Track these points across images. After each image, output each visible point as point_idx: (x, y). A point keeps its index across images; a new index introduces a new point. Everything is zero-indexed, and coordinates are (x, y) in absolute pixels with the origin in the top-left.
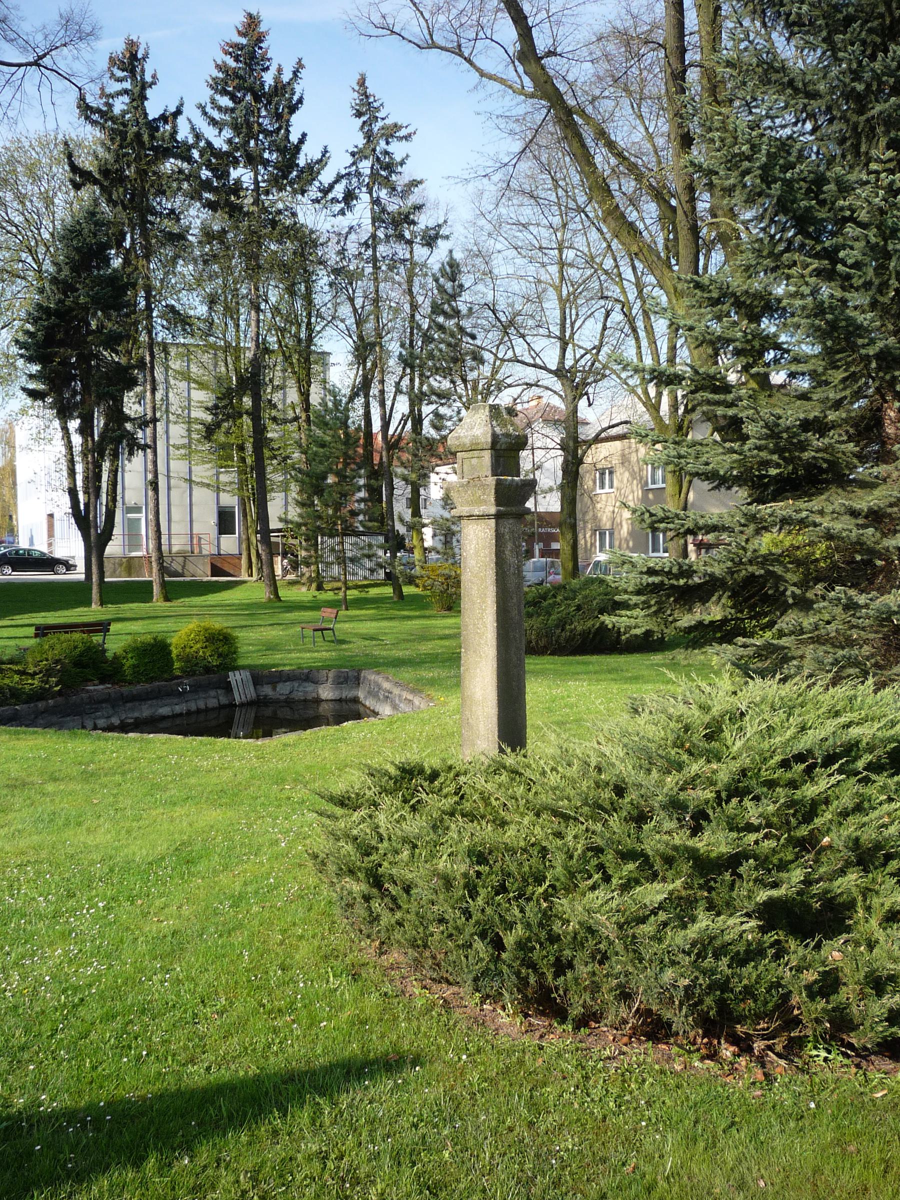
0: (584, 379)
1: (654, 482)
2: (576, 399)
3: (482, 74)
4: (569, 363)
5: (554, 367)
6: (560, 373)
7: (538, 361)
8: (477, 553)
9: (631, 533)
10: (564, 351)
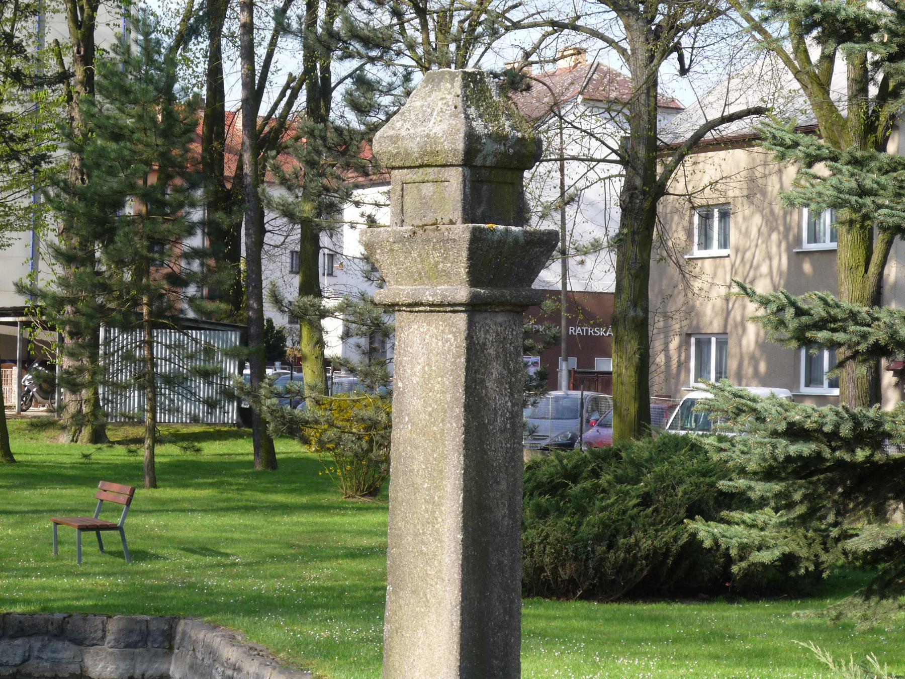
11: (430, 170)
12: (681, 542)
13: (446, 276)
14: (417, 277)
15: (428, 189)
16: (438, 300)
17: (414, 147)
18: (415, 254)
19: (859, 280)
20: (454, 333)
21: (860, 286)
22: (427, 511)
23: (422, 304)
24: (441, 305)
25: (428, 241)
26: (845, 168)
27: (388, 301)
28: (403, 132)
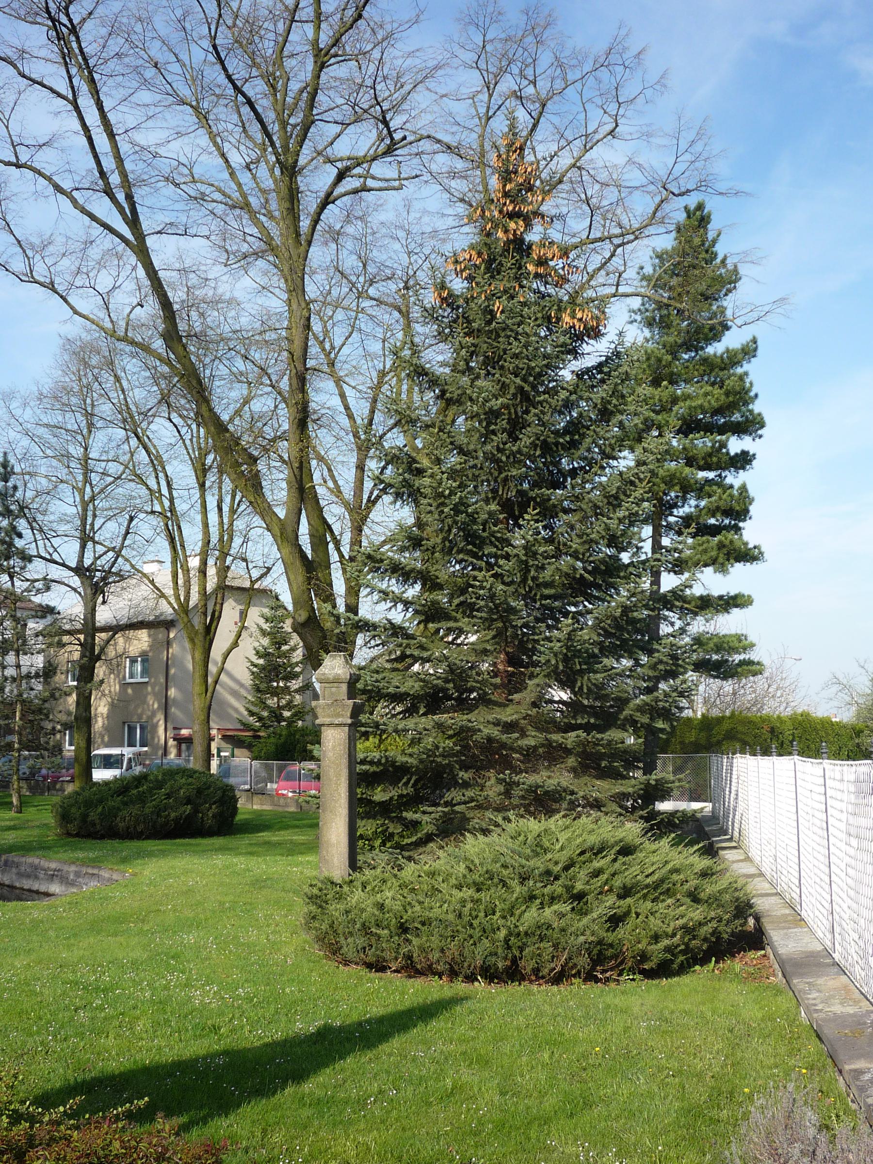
0: (104, 579)
1: (131, 677)
2: (95, 595)
3: (76, 312)
4: (87, 562)
5: (73, 565)
6: (79, 570)
7: (56, 557)
8: (334, 747)
9: (106, 728)
10: (83, 547)
14: (329, 716)
15: (333, 690)
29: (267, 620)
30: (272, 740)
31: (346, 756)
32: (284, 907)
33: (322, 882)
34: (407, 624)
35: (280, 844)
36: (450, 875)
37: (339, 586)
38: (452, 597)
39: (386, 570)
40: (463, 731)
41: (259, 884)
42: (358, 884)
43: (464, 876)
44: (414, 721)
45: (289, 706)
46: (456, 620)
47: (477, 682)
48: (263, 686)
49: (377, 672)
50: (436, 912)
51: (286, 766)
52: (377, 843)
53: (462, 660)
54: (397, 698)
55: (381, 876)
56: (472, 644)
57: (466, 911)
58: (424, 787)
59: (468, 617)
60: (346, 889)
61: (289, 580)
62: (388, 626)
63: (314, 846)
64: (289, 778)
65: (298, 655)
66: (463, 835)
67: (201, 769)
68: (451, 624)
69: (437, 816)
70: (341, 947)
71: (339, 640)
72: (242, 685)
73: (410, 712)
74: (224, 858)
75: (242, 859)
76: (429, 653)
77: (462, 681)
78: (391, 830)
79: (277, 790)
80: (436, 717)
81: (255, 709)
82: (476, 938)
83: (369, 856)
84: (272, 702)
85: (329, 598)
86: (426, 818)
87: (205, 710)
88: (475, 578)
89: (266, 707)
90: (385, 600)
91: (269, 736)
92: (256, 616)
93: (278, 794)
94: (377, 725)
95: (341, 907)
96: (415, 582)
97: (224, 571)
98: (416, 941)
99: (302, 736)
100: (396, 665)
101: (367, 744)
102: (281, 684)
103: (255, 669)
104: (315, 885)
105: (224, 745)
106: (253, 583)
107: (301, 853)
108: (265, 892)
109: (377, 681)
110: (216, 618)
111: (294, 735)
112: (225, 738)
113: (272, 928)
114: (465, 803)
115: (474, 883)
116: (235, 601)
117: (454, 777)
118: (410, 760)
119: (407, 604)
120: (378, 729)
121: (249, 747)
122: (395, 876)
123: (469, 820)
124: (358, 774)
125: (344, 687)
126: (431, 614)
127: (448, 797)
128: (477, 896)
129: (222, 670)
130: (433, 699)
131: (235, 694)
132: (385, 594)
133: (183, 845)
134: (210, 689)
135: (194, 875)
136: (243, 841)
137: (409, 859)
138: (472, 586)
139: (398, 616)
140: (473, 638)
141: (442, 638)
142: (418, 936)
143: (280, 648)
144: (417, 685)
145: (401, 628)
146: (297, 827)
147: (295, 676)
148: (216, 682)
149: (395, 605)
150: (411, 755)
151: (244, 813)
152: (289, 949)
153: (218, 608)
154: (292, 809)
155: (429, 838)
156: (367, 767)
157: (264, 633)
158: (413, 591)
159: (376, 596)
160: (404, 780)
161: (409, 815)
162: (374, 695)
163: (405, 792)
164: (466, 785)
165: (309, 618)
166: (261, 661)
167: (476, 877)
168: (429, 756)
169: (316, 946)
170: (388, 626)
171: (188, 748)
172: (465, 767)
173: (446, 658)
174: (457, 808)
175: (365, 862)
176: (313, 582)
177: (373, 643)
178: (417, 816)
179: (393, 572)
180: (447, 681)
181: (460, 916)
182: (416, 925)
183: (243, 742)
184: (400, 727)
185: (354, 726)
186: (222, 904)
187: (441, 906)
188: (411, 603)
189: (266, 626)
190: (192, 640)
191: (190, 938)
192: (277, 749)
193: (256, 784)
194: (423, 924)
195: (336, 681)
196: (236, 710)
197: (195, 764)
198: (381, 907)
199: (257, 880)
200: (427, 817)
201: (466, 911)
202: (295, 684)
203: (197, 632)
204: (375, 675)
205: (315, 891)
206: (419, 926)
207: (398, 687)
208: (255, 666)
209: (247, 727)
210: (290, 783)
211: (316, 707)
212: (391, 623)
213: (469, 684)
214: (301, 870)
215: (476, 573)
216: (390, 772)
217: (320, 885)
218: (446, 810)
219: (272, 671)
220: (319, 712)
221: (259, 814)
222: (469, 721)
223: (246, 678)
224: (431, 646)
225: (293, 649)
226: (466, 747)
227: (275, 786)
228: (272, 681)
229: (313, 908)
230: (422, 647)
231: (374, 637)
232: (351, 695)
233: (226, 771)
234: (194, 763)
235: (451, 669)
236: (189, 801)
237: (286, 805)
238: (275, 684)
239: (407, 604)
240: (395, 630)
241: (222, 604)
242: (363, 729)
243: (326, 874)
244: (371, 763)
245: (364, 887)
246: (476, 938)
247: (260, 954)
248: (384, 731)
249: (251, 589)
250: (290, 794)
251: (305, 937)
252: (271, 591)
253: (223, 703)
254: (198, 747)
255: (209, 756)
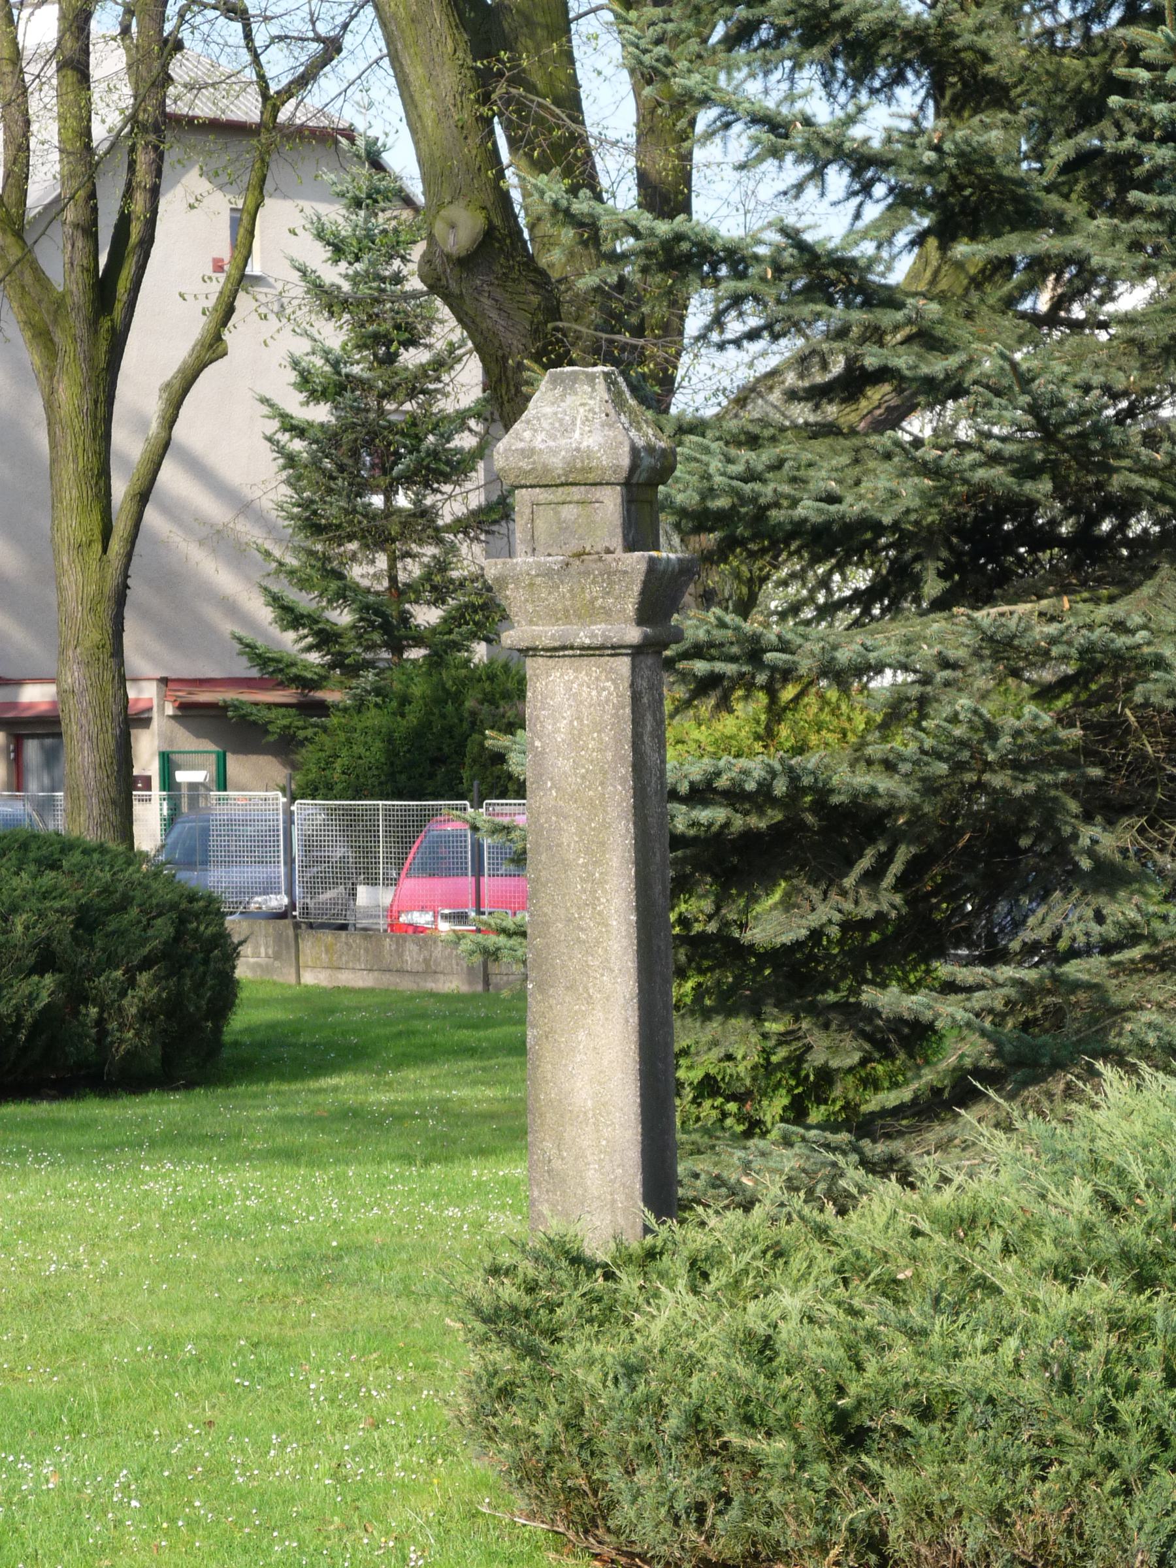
8: (575, 738)
11: (574, 489)
12: (38, 1006)
13: (607, 614)
14: (554, 616)
15: (569, 512)
16: (598, 641)
17: (557, 463)
18: (564, 589)
19: (94, 565)
20: (614, 681)
21: (96, 576)
22: (584, 891)
23: (572, 648)
24: (602, 647)
25: (587, 573)
26: (715, 446)
27: (523, 645)
28: (538, 444)
29: (338, 249)
30: (373, 718)
31: (625, 770)
32: (404, 1353)
33: (538, 1258)
34: (868, 248)
35: (397, 1117)
36: (1033, 1227)
37: (609, 104)
38: (1043, 132)
39: (782, 33)
40: (1100, 668)
41: (316, 1267)
42: (677, 1265)
43: (1088, 1230)
44: (898, 629)
45: (436, 586)
46: (1063, 227)
47: (1148, 470)
48: (331, 511)
49: (753, 441)
50: (975, 1369)
51: (425, 817)
52: (774, 1107)
53: (1087, 388)
54: (837, 541)
55: (768, 1234)
56: (1127, 320)
57: (1090, 1363)
58: (951, 890)
59: (1112, 211)
60: (629, 1283)
61: (403, 83)
62: (789, 256)
63: (510, 1130)
64: (434, 867)
65: (467, 383)
66: (1092, 1074)
67: (91, 837)
68: (1046, 242)
69: (997, 999)
70: (613, 1504)
71: (612, 321)
72: (245, 508)
73: (893, 589)
74: (181, 1174)
75: (250, 1175)
76: (953, 361)
77: (1086, 467)
78: (818, 1058)
79: (392, 913)
80: (986, 616)
81: (305, 601)
82: (1129, 1467)
83: (731, 1161)
84: (367, 571)
85: (569, 155)
86: (951, 1010)
87: (106, 610)
88: (1134, 56)
89: (346, 593)
90: (775, 153)
91: (360, 706)
92: (293, 234)
93: (395, 927)
94: (754, 652)
95: (610, 1351)
96: (899, 79)
97: (155, 56)
98: (896, 1481)
99: (489, 699)
100: (831, 411)
101: (728, 724)
102: (403, 500)
103: (297, 445)
104: (510, 1271)
105: (185, 740)
106: (271, 102)
107: (483, 1152)
108: (334, 1299)
109: (750, 476)
110: (133, 244)
111: (457, 698)
112: (189, 713)
113: (357, 1434)
114: (1108, 948)
115: (1125, 1255)
116: (212, 175)
117: (1061, 849)
118: (884, 783)
119: (863, 164)
120: (757, 669)
121: (285, 746)
122: (821, 1232)
123: (1118, 1012)
124: (677, 841)
125: (611, 502)
126: (963, 203)
127: (1035, 930)
128: (1135, 1305)
129: (163, 447)
130: (972, 547)
131: (217, 540)
132: (774, 127)
133: (28, 1125)
134: (121, 527)
135: (65, 1238)
136: (259, 1107)
137: (881, 1168)
138: (1126, 88)
139: (829, 216)
140: (1132, 298)
141: (1010, 302)
142: (904, 1460)
143: (391, 358)
144: (911, 490)
145: (844, 265)
146: (470, 1051)
147: (451, 468)
148: (143, 497)
149: (818, 174)
150: (889, 766)
151: (265, 1003)
152: (416, 1514)
153: (139, 205)
154: (453, 984)
155: (961, 1092)
156: (714, 815)
157: (330, 301)
158: (894, 113)
159: (741, 140)
160: (865, 863)
161: (889, 999)
162: (746, 533)
163: (868, 909)
164: (1108, 877)
165: (489, 234)
166: (321, 413)
167: (1133, 1232)
168: (959, 767)
169: (521, 1503)
170: (789, 256)
171: (52, 758)
172: (1104, 806)
173: (1025, 380)
174: (1074, 969)
175: (717, 1182)
176: (501, 89)
177: (735, 327)
178: (915, 1003)
179: (808, 42)
180: (1027, 470)
181: (1066, 1383)
182: (898, 1418)
183: (261, 729)
184: (844, 656)
185: (654, 654)
186: (166, 1344)
187: (992, 1348)
188: (883, 163)
189: (335, 275)
190: (43, 337)
191: (47, 1474)
192: (392, 753)
193: (312, 888)
194: (925, 1413)
195: (579, 478)
196: (231, 608)
197: (71, 815)
198: (762, 1350)
199: (306, 1256)
200: (958, 1005)
201: (1090, 1363)
202: (455, 502)
203: (59, 306)
204: (745, 454)
205: (509, 1292)
206: (910, 1423)
207: (832, 499)
208: (299, 431)
209: (272, 668)
210: (441, 886)
211: (502, 580)
212: (802, 247)
213: (1116, 482)
214: (470, 1215)
215: (1137, 33)
216: (811, 833)
217: (527, 1268)
218: (1029, 975)
219: (365, 453)
220: (514, 598)
221: (322, 1003)
222: (1120, 627)
223: (267, 484)
224: (962, 331)
225: (442, 364)
226: (1110, 730)
227: (386, 896)
228: (362, 488)
229: (502, 1357)
230: (927, 339)
231: (737, 300)
232: (638, 532)
233: (193, 840)
234: (71, 817)
235: (1043, 416)
236: (46, 961)
237: (429, 970)
238: (378, 501)
239: (863, 164)
240: (821, 275)
241: (155, 193)
242: (700, 667)
243: (554, 1226)
244: (734, 797)
245: (699, 1271)
246: (1129, 1467)
247: (306, 1531)
248: (787, 674)
249: (269, 123)
250: (444, 926)
251: (479, 1467)
252: (349, 134)
253: (174, 581)
254: (83, 754)
255: (124, 784)
